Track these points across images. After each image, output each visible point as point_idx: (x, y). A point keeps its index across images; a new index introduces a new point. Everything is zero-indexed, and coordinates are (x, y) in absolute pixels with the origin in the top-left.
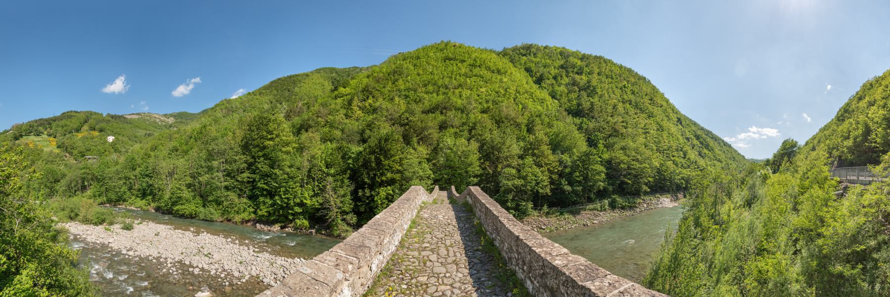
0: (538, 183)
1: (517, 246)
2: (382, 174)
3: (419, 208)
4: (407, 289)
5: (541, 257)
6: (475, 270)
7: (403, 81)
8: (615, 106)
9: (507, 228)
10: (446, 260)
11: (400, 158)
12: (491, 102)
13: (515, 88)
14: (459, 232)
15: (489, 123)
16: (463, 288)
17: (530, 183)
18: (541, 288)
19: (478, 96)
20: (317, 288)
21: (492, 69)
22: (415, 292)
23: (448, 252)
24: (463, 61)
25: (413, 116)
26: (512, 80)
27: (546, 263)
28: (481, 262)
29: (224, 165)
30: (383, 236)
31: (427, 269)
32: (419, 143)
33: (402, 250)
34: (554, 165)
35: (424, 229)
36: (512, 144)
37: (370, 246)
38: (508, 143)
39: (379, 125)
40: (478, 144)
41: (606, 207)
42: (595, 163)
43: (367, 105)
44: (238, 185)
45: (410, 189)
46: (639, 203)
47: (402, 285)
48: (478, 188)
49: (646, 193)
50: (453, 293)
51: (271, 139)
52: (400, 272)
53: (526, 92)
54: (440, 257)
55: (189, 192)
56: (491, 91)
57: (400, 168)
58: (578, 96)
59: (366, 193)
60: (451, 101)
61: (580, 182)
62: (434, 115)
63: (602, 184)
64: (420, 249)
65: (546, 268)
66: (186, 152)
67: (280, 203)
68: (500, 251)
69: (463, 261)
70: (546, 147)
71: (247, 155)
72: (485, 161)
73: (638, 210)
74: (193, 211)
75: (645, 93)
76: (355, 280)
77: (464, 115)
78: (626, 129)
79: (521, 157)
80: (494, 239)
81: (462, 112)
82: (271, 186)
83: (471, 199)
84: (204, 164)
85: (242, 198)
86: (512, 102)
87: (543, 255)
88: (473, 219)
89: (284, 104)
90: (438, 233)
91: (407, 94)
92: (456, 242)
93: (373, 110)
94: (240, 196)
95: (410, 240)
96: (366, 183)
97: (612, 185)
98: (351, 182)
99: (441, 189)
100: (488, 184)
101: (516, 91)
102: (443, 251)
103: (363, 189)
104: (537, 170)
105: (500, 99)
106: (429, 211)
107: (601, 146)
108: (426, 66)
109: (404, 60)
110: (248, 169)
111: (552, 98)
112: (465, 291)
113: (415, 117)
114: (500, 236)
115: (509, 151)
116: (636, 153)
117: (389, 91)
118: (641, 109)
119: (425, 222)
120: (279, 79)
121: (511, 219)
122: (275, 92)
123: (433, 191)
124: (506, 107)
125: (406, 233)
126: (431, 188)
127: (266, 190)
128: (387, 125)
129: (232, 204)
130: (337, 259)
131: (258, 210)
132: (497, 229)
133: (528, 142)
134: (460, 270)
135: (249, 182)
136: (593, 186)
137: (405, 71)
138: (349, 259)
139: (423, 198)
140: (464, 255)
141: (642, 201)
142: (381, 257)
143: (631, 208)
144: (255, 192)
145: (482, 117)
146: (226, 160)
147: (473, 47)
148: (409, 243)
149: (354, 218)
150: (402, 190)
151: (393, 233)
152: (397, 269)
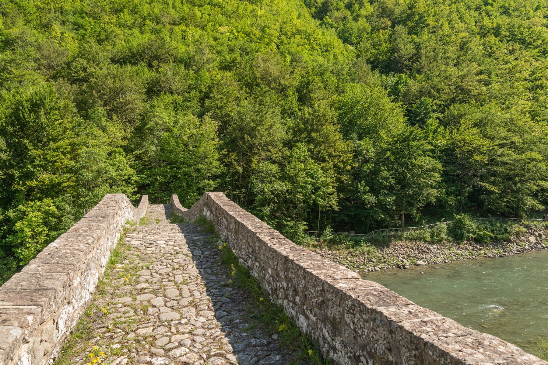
0: (316, 189)
1: (287, 270)
2: (28, 176)
3: (122, 232)
4: (121, 348)
8: (465, 44)
9: (270, 248)
10: (178, 303)
11: (70, 144)
12: (237, 51)
14: (195, 262)
15: (234, 88)
16: (208, 334)
17: (302, 187)
19: (216, 39)
22: (136, 349)
25: (97, 65)
26: (274, 12)
27: (326, 287)
28: (232, 300)
30: (72, 272)
31: (150, 317)
32: (110, 117)
33: (103, 298)
34: (344, 157)
35: (136, 262)
36: (275, 122)
37: (54, 286)
38: (268, 120)
39: (22, 76)
40: (217, 124)
41: (443, 235)
42: (420, 155)
46: (517, 234)
48: (221, 194)
49: (533, 213)
50: (194, 341)
52: (105, 329)
53: (299, 32)
54: (168, 300)
56: (238, 32)
57: (73, 163)
58: (391, 36)
61: (391, 188)
62: (135, 68)
63: (434, 191)
65: (326, 294)
68: (259, 283)
69: (206, 302)
70: (333, 128)
72: (228, 151)
73: (514, 247)
75: (535, 5)
77: (191, 73)
78: (486, 85)
79: (289, 144)
80: (250, 268)
81: (188, 66)
83: (212, 212)
86: (275, 49)
87: (322, 277)
88: (215, 242)
90: (160, 267)
91: (80, 21)
92: (192, 277)
95: (114, 281)
97: (458, 193)
99: (153, 201)
100: (234, 190)
101: (281, 31)
102: (172, 292)
104: (313, 165)
106: (141, 236)
107: (432, 122)
111: (344, 42)
112: (213, 337)
114: (258, 262)
115: (269, 135)
116: (508, 131)
118: (523, 41)
119: (136, 253)
121: (277, 235)
124: (263, 60)
132: (254, 251)
133: (301, 119)
134: (201, 313)
136: (417, 194)
138: (23, 309)
140: (205, 294)
141: (524, 230)
142: (70, 308)
143: (496, 241)
145: (222, 77)
148: (113, 287)
151: (86, 270)
152: (100, 326)
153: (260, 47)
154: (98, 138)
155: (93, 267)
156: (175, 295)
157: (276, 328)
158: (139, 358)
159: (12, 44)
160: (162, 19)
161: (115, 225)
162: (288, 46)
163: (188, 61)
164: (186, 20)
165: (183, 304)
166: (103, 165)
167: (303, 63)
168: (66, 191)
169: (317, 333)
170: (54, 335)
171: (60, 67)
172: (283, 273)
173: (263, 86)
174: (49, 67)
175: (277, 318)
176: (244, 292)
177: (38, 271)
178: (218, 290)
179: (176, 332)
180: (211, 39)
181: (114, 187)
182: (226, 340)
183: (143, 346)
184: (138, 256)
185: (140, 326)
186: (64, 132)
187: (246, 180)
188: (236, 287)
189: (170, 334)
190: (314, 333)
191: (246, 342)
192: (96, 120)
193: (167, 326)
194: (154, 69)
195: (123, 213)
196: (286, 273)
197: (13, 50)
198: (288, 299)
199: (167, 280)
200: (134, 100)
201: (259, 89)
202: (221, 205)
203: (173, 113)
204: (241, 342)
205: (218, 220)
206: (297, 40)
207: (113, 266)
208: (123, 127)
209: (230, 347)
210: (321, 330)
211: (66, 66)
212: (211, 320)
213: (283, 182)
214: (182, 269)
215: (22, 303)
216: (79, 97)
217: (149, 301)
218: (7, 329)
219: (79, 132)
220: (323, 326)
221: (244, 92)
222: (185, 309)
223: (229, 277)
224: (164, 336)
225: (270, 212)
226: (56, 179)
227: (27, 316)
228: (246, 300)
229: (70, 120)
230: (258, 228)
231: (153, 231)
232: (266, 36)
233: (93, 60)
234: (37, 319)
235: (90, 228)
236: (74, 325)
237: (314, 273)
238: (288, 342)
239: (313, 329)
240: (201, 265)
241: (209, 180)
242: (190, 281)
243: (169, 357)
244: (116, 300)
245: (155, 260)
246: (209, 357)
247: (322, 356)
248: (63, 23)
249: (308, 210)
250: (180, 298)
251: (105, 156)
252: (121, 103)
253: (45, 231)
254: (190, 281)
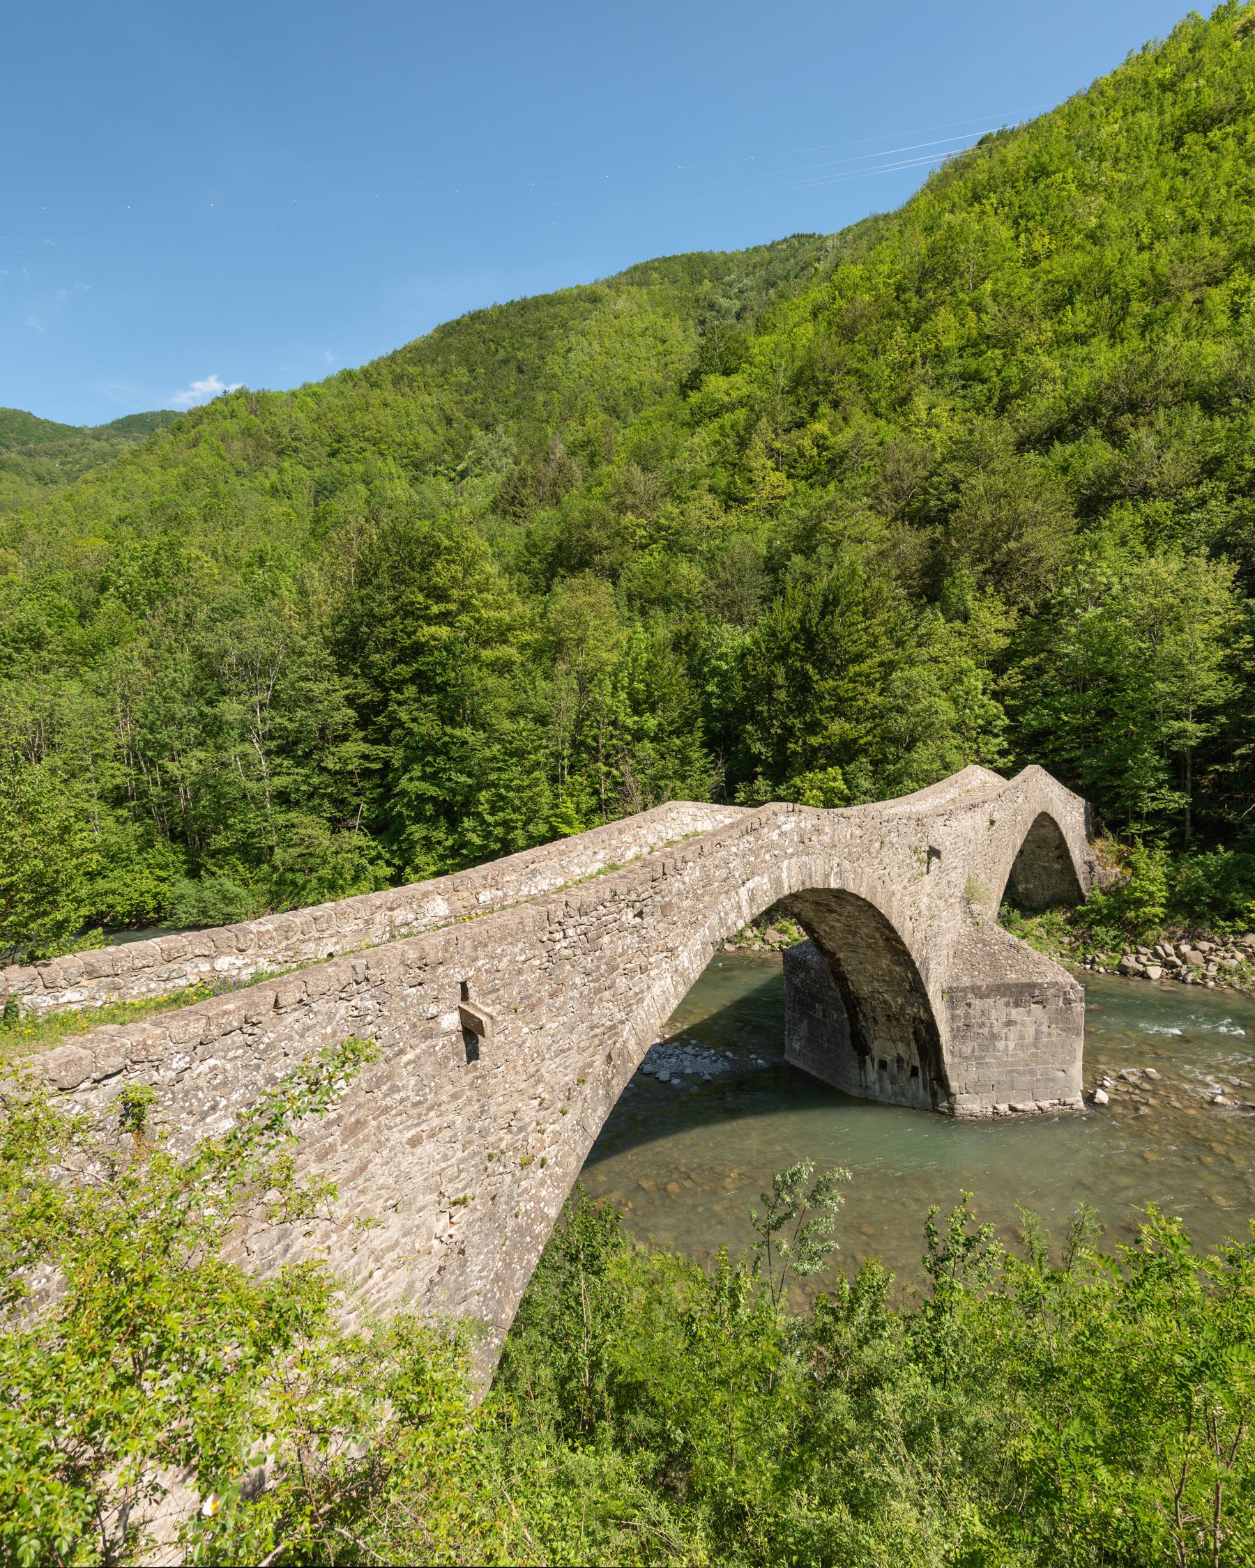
2: (813, 727)
11: (881, 664)
29: (266, 714)
43: (807, 443)
44: (327, 786)
51: (444, 618)
55: (120, 821)
66: (90, 652)
67: (478, 841)
71: (356, 676)
74: (148, 898)
82: (448, 784)
84: (180, 710)
85: (345, 833)
89: (500, 429)
91: (973, 364)
93: (829, 461)
94: (336, 825)
96: (757, 759)
110: (362, 723)
120: (476, 317)
122: (461, 375)
127: (433, 799)
129: (311, 855)
131: (408, 870)
135: (366, 774)
144: (392, 809)
146: (275, 698)
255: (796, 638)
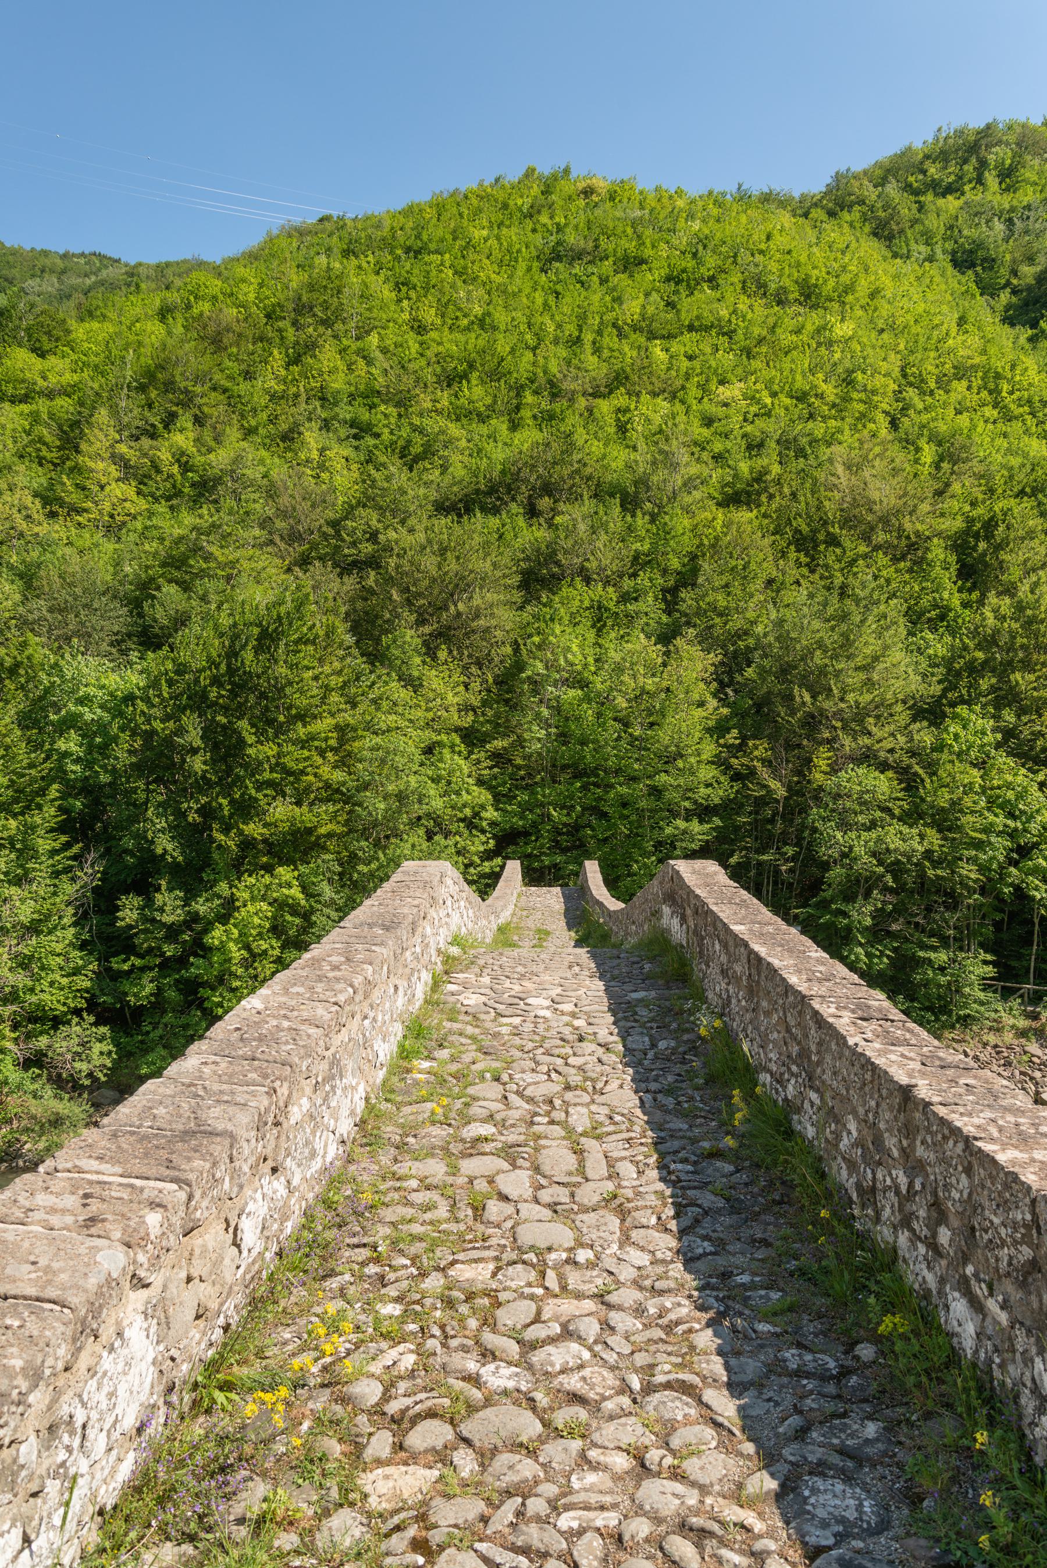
0: (1024, 851)
1: (909, 1131)
2: (246, 809)
3: (439, 968)
4: (402, 1320)
5: (1023, 1183)
6: (706, 1238)
7: (343, 351)
9: (853, 1051)
10: (572, 1195)
11: (338, 728)
13: (894, 364)
14: (631, 1071)
16: (652, 1311)
17: (979, 845)
18: (1020, 1334)
19: (708, 421)
20: (16, 1323)
21: (773, 286)
22: (442, 1327)
23: (581, 1162)
24: (631, 264)
25: (403, 522)
26: (881, 324)
28: (734, 1206)
30: (286, 1085)
32: (430, 652)
33: (372, 1155)
35: (467, 1058)
37: (230, 1127)
38: (868, 644)
39: (233, 564)
45: (395, 878)
47: (379, 1306)
48: (711, 867)
50: (607, 1327)
53: (961, 372)
54: (543, 1182)
56: (774, 395)
57: (338, 776)
59: (162, 910)
60: (576, 457)
62: (494, 522)
64: (455, 1148)
68: (820, 1159)
69: (652, 1200)
72: (744, 738)
76: (173, 1290)
80: (792, 1107)
81: (630, 503)
83: (683, 919)
86: (884, 433)
88: (691, 1012)
90: (529, 1077)
91: (365, 416)
95: (407, 1110)
98: (76, 849)
99: (534, 877)
100: (761, 851)
101: (905, 376)
103: (144, 888)
105: (818, 429)
106: (486, 980)
108: (453, 286)
109: (347, 253)
113: (411, 531)
115: (869, 684)
117: (274, 397)
119: (470, 1030)
121: (880, 1010)
123: (493, 886)
124: (848, 467)
125: (385, 1082)
126: (482, 876)
128: (270, 564)
130: (86, 1196)
132: (804, 1053)
134: (635, 1234)
137: (353, 307)
139: (456, 918)
140: (654, 1174)
142: (279, 1185)
145: (727, 525)
147: (679, 193)
148: (402, 1126)
149: (97, 1047)
150: (355, 884)
151: (330, 1078)
152: (355, 1240)
153: (840, 431)
154: (400, 709)
155: (350, 1067)
156: (565, 1168)
157: (869, 1321)
158: (446, 1359)
159: (214, 487)
160: (564, 386)
161: (418, 949)
162: (925, 417)
163: (632, 490)
164: (627, 378)
165: (586, 1201)
166: (413, 780)
167: (975, 462)
168: (324, 849)
169: (1011, 1368)
170: (227, 1261)
171: (316, 536)
172: (894, 1140)
173: (847, 544)
174: (293, 537)
175: (874, 1288)
176: (771, 1183)
177: (201, 1078)
178: (690, 1168)
179: (557, 1290)
180: (696, 423)
181: (436, 838)
182: (706, 1339)
183: (462, 1320)
184: (473, 1038)
185: (461, 1256)
186: (324, 697)
187: (798, 820)
188: (747, 1164)
189: (540, 1291)
190: (1000, 1366)
191: (767, 1355)
192: (398, 662)
193: (533, 1266)
194: (542, 520)
195: (442, 913)
196: (905, 1143)
197: (216, 502)
198: (913, 1231)
199: (546, 1120)
200: (491, 606)
201: (838, 551)
202: (710, 901)
203: (591, 635)
204: (753, 1354)
205: (701, 945)
206: (953, 397)
207: (405, 1064)
208: (463, 678)
209: (716, 1366)
210: (1028, 1362)
211: (330, 531)
212: (663, 1261)
213: (911, 826)
214: (590, 1089)
215: (144, 1170)
216: (359, 605)
217: (491, 1181)
218: (91, 1248)
219: (356, 695)
220: (1034, 1350)
221: (791, 564)
222: (590, 1218)
223: (726, 1127)
224: (522, 1296)
225: (873, 918)
226: (304, 815)
227: (147, 1210)
228: (776, 1209)
229: (337, 665)
230: (820, 981)
231: (520, 969)
232: (855, 395)
233: (392, 510)
234: (174, 1220)
235: (348, 960)
236: (289, 1231)
237: (1002, 1158)
238: (911, 1380)
239: (996, 1350)
240: (647, 1080)
241: (687, 820)
242: (611, 1128)
243: (530, 1367)
244: (406, 1167)
245: (518, 1054)
246: (649, 1389)
247: (1030, 1458)
248: (326, 425)
249: (998, 917)
250: (579, 1179)
251: (418, 757)
252: (459, 614)
253: (272, 947)
254: (611, 1128)
255: (216, 681)
